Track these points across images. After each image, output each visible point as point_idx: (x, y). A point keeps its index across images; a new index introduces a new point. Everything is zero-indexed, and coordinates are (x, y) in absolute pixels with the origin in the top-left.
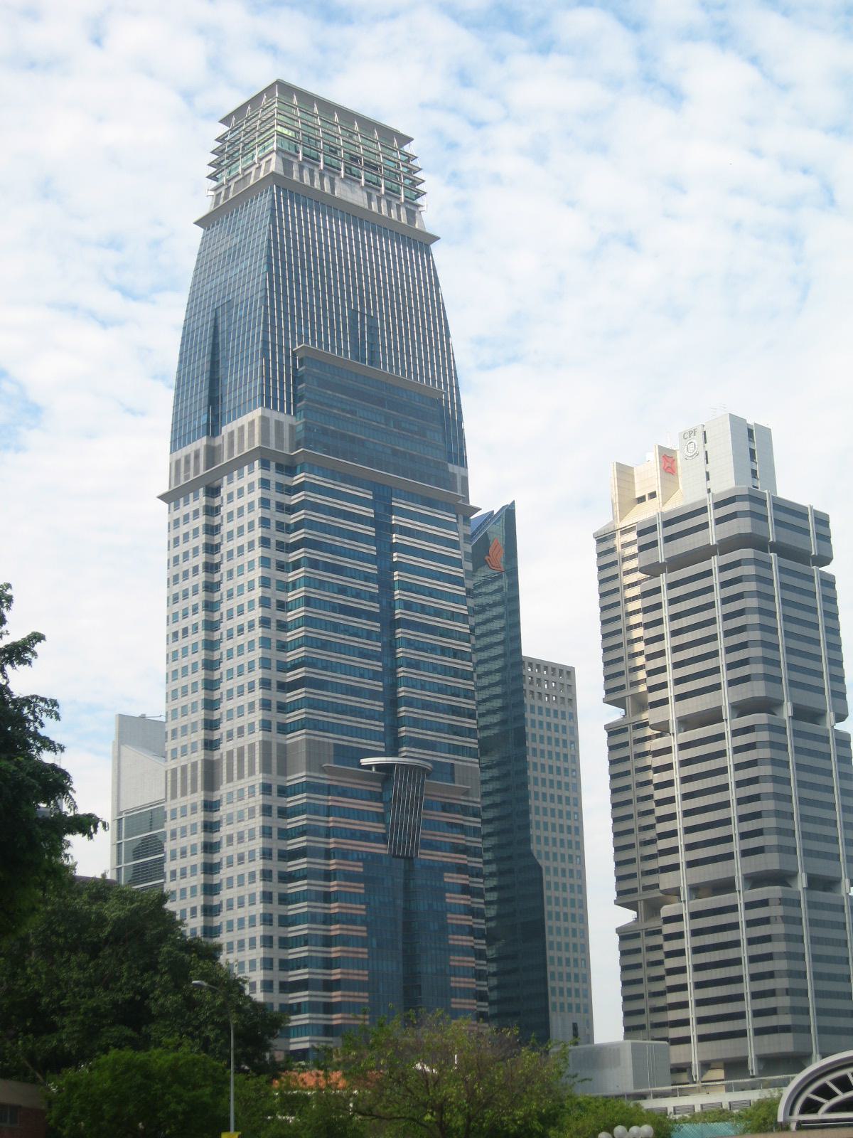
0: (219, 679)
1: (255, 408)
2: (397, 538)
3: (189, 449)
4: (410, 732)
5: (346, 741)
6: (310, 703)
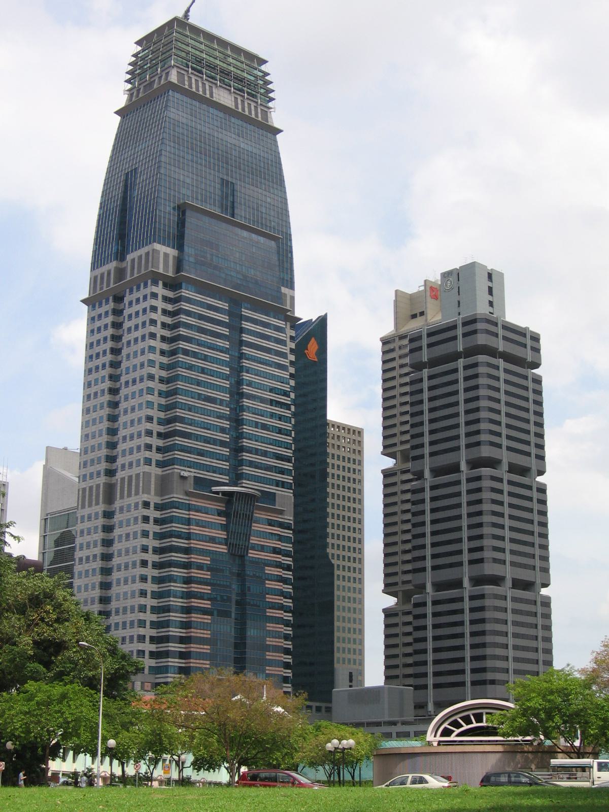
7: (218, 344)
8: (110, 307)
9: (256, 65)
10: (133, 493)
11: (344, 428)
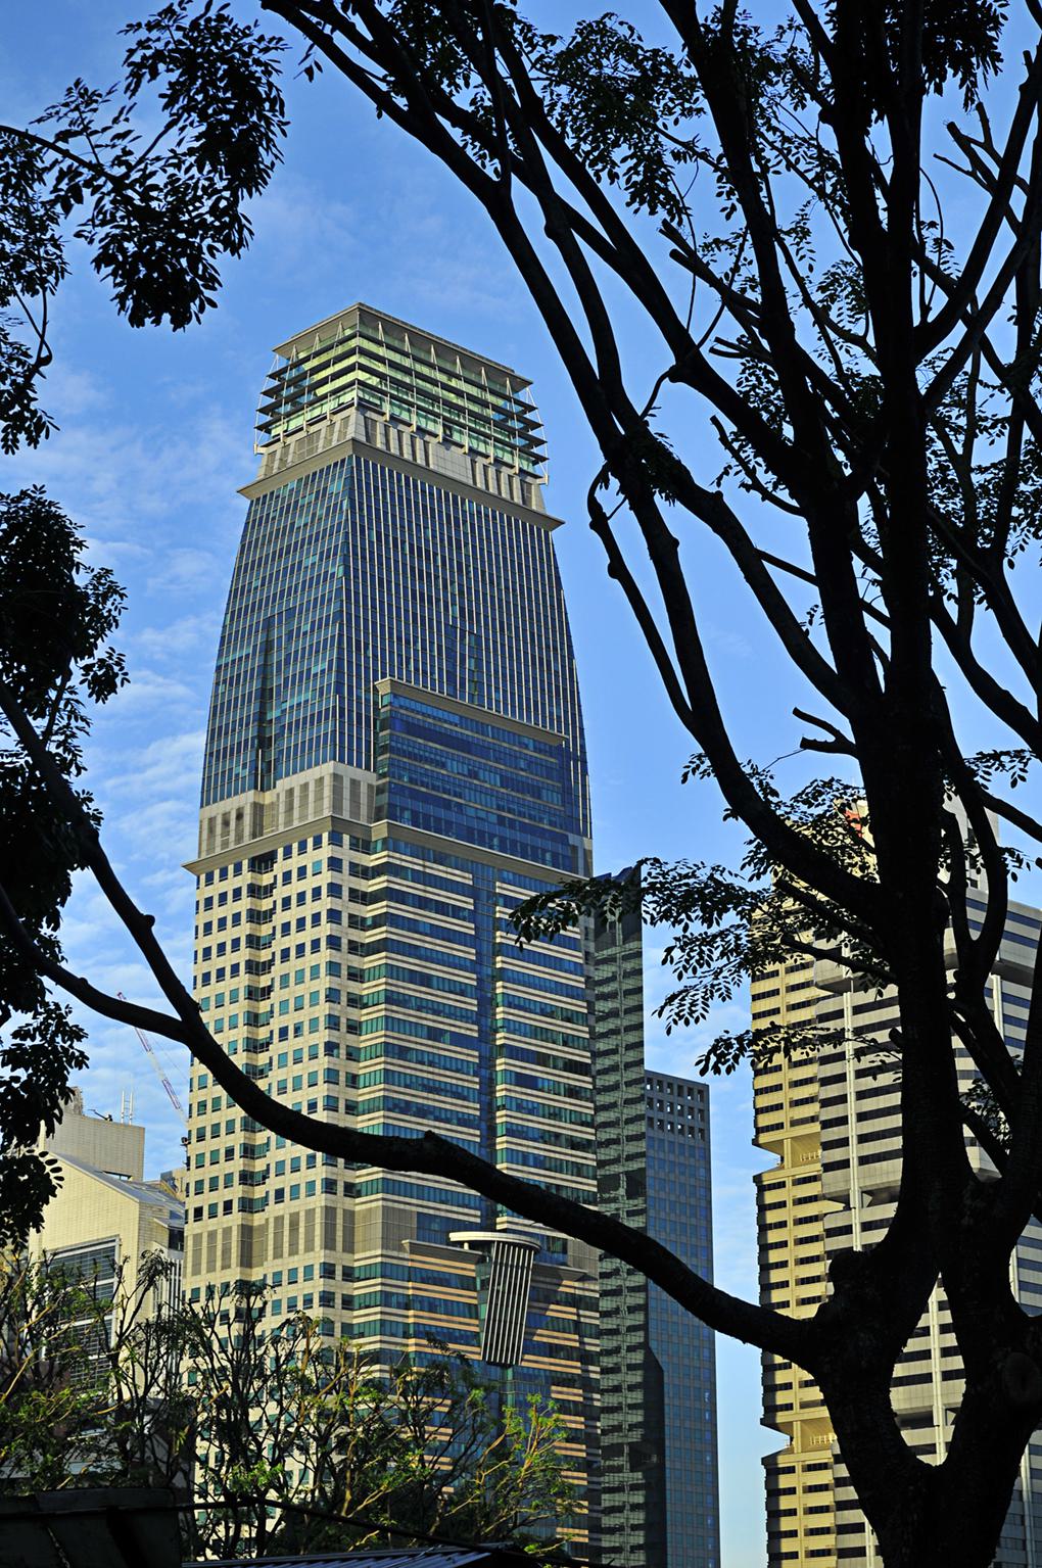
0: (272, 885)
1: (324, 761)
2: (503, 962)
3: (230, 805)
4: (511, 1117)
5: (433, 1208)
6: (388, 894)
7: (455, 953)
8: (243, 880)
9: (508, 391)
10: (301, 1247)
11: (670, 1085)
